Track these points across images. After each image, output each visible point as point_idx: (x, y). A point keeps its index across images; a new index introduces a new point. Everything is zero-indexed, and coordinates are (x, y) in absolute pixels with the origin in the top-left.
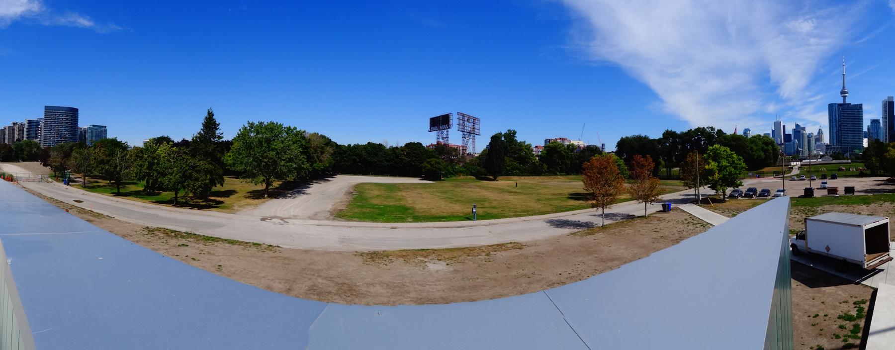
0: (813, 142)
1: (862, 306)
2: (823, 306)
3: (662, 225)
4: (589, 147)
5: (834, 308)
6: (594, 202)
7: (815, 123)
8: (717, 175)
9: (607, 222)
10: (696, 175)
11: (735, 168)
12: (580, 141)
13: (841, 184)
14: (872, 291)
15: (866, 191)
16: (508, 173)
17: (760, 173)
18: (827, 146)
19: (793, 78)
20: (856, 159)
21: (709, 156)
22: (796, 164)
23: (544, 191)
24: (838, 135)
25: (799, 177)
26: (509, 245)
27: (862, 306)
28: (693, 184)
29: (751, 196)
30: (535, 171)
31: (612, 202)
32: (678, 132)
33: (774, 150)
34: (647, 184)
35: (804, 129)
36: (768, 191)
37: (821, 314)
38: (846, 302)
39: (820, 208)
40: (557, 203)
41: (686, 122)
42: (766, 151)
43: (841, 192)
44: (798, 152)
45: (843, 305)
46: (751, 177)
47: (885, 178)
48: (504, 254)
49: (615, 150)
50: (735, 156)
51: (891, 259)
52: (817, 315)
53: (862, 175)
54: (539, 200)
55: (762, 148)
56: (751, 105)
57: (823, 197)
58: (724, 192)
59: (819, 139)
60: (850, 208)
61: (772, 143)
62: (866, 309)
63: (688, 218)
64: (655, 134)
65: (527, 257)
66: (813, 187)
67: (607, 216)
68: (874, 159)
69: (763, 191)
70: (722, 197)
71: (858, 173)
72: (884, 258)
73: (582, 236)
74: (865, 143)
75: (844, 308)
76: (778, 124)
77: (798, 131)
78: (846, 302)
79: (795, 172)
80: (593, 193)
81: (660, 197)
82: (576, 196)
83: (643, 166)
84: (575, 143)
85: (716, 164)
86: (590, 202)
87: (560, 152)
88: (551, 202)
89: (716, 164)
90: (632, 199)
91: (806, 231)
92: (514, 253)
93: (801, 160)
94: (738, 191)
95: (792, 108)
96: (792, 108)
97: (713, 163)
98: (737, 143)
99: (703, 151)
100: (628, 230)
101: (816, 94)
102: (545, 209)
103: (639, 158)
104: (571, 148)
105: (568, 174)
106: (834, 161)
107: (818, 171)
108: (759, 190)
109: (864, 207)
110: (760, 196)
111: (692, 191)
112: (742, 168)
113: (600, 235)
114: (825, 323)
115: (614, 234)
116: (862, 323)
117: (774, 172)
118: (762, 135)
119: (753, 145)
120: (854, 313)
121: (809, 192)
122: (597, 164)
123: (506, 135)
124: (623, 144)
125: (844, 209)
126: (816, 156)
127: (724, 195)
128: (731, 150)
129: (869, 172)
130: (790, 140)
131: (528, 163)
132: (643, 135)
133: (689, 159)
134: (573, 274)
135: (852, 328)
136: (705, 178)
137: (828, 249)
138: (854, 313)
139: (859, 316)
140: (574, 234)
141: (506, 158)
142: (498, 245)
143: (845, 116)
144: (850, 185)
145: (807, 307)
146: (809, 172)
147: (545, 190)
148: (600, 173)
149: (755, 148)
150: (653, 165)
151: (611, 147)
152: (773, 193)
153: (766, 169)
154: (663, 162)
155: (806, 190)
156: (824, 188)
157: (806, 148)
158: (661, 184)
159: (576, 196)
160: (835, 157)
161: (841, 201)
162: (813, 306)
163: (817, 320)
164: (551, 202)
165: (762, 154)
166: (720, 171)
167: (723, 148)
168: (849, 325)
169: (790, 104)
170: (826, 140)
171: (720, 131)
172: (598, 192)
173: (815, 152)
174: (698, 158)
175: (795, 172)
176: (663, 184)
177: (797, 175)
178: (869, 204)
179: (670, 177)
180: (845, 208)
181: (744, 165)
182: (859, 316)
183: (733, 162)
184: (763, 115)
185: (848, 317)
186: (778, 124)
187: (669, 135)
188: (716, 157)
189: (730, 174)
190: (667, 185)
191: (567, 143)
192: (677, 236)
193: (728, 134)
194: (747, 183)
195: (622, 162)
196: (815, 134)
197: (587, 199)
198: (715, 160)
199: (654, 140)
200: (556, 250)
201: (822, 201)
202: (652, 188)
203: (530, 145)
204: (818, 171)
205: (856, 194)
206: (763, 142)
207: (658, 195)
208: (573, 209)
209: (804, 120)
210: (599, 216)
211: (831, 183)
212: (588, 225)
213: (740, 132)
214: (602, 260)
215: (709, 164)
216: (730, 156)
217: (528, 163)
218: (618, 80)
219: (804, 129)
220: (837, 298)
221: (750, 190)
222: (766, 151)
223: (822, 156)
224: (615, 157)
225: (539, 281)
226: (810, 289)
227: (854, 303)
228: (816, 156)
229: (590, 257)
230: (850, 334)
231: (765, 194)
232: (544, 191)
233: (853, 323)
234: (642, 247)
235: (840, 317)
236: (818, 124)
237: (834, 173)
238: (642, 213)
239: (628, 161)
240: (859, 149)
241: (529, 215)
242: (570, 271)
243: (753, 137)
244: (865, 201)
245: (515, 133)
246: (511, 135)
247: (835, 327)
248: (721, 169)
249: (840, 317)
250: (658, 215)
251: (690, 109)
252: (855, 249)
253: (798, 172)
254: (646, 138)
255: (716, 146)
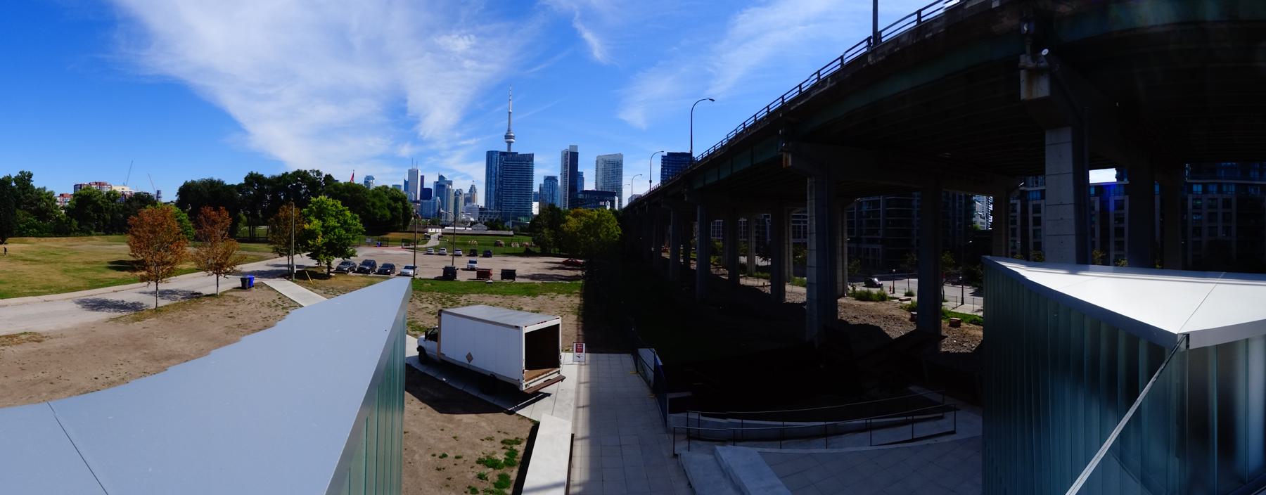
0: (461, 202)
1: (515, 447)
2: (454, 443)
3: (240, 308)
4: (137, 195)
5: (473, 446)
6: (144, 273)
7: (467, 177)
8: (320, 240)
9: (163, 303)
10: (290, 237)
11: (348, 230)
12: (124, 186)
13: (496, 265)
14: (531, 425)
15: (533, 277)
16: (22, 233)
17: (383, 240)
18: (481, 209)
19: (439, 110)
20: (522, 230)
21: (311, 211)
22: (435, 232)
23: (73, 258)
24: (497, 196)
25: (439, 251)
26: (23, 337)
27: (515, 447)
28: (285, 250)
29: (367, 272)
30: (60, 230)
31: (170, 273)
32: (267, 175)
33: (406, 209)
34: (221, 248)
35: (450, 183)
36: (392, 267)
37: (451, 455)
38: (491, 439)
39: (464, 297)
40: (90, 275)
41: (281, 163)
42: (393, 210)
43: (496, 276)
44: (440, 214)
45: (485, 443)
46: (369, 245)
47: (561, 260)
48: (17, 349)
49: (175, 199)
50: (348, 213)
51: (562, 379)
52: (444, 456)
53: (528, 253)
54: (66, 271)
55: (389, 205)
56: (377, 144)
57: (470, 282)
58: (329, 263)
59: (470, 199)
60: (508, 300)
61: (403, 199)
62: (521, 453)
63: (276, 298)
64: (234, 177)
65: (49, 354)
66: (457, 265)
67: (163, 294)
68: (545, 231)
69: (385, 265)
70: (326, 271)
71: (522, 250)
72: (552, 377)
73: (126, 322)
74: (535, 208)
75: (487, 448)
76: (413, 173)
77: (442, 185)
78: (491, 439)
79: (433, 242)
80: (143, 261)
81: (238, 268)
82: (119, 266)
83: (214, 222)
84: (119, 189)
85: (321, 223)
86: (138, 274)
87: (95, 203)
88: (83, 274)
89: (321, 223)
90: (198, 270)
91: (439, 328)
92: (30, 347)
93: (443, 227)
94: (348, 263)
95: (435, 153)
96: (435, 153)
97: (316, 222)
98: (353, 195)
99: (302, 203)
100: (192, 315)
101: (470, 137)
102: (75, 284)
103: (208, 210)
104: (112, 196)
105: (107, 233)
106: (490, 232)
107: (465, 244)
108: (379, 265)
109: (528, 299)
110: (380, 272)
111: (283, 260)
112: (358, 230)
113: (152, 322)
114: (456, 468)
115: (172, 319)
116: (513, 474)
117: (403, 241)
118: (390, 186)
119: (376, 200)
120: (501, 456)
121: (450, 273)
122: (148, 219)
123: (16, 179)
124: (187, 192)
125: (498, 301)
126: (464, 223)
127: (329, 268)
128: (343, 205)
129: (538, 250)
130: (430, 197)
131: (50, 218)
132: (216, 178)
133: (282, 214)
134: (112, 378)
135: (496, 479)
136: (303, 242)
137: (470, 357)
138: (501, 456)
139: (509, 463)
140: (116, 319)
141: (18, 211)
142: (7, 337)
143: (508, 170)
144: (509, 267)
145: (432, 441)
146: (453, 244)
147: (76, 257)
148: (153, 232)
149: (378, 204)
150: (229, 221)
151: (169, 195)
152: (399, 269)
153: (391, 235)
154: (244, 218)
155: (446, 270)
156: (473, 269)
157: (452, 210)
158: (239, 249)
159: (119, 266)
160: (492, 225)
161: (492, 289)
162: (441, 440)
163: (444, 463)
164: (83, 274)
165: (388, 213)
166: (325, 233)
167: (331, 202)
168: (492, 474)
169: (433, 147)
170: (480, 201)
171: (329, 177)
172: (149, 258)
173: (464, 217)
174: (294, 212)
175: (433, 242)
176: (243, 249)
177: (435, 248)
178: (535, 295)
179: (253, 239)
180: (499, 299)
181: (360, 226)
182: (509, 463)
183: (345, 222)
184: (390, 159)
185: (492, 463)
186: (413, 173)
187: (253, 179)
188: (321, 213)
189: (339, 238)
190: (249, 250)
191: (106, 189)
192: (261, 324)
193: (342, 181)
194: (363, 253)
195: (184, 216)
196: (466, 191)
197: (135, 270)
198: (318, 217)
199: (232, 186)
200: (91, 344)
201: (467, 288)
202: (226, 255)
203: (52, 193)
204: (465, 244)
205: (517, 280)
206: (393, 197)
207: (235, 264)
208: (114, 284)
209: (452, 170)
210: (151, 293)
211: (482, 263)
212: (135, 307)
213: (359, 180)
214: (155, 359)
215: (309, 222)
216: (341, 213)
217: (50, 218)
218: (181, 103)
219: (450, 183)
220: (478, 431)
221: (366, 263)
222: (393, 210)
223: (473, 224)
224: (176, 210)
225: (66, 388)
226: (438, 415)
227: (503, 442)
228: (464, 223)
229: (138, 354)
230: (493, 488)
231: (387, 270)
232: (73, 258)
233: (499, 472)
234: (210, 340)
235: (480, 462)
236: (470, 178)
237: (488, 248)
238: (212, 290)
239: (193, 216)
240: (526, 216)
241: (52, 293)
242: (108, 373)
243: (377, 188)
244: (529, 291)
245: (30, 175)
246: (25, 179)
247: (471, 475)
248: (327, 230)
249: (480, 462)
250: (234, 294)
251: (286, 144)
252: (510, 362)
253: (438, 243)
254: (220, 183)
255: (323, 198)
